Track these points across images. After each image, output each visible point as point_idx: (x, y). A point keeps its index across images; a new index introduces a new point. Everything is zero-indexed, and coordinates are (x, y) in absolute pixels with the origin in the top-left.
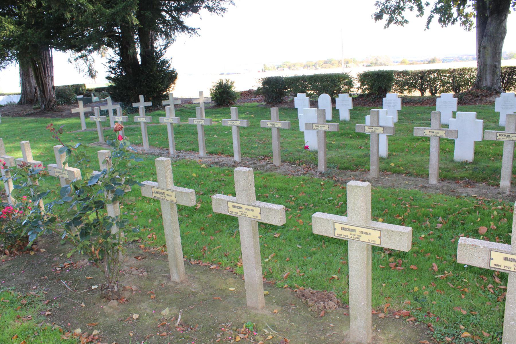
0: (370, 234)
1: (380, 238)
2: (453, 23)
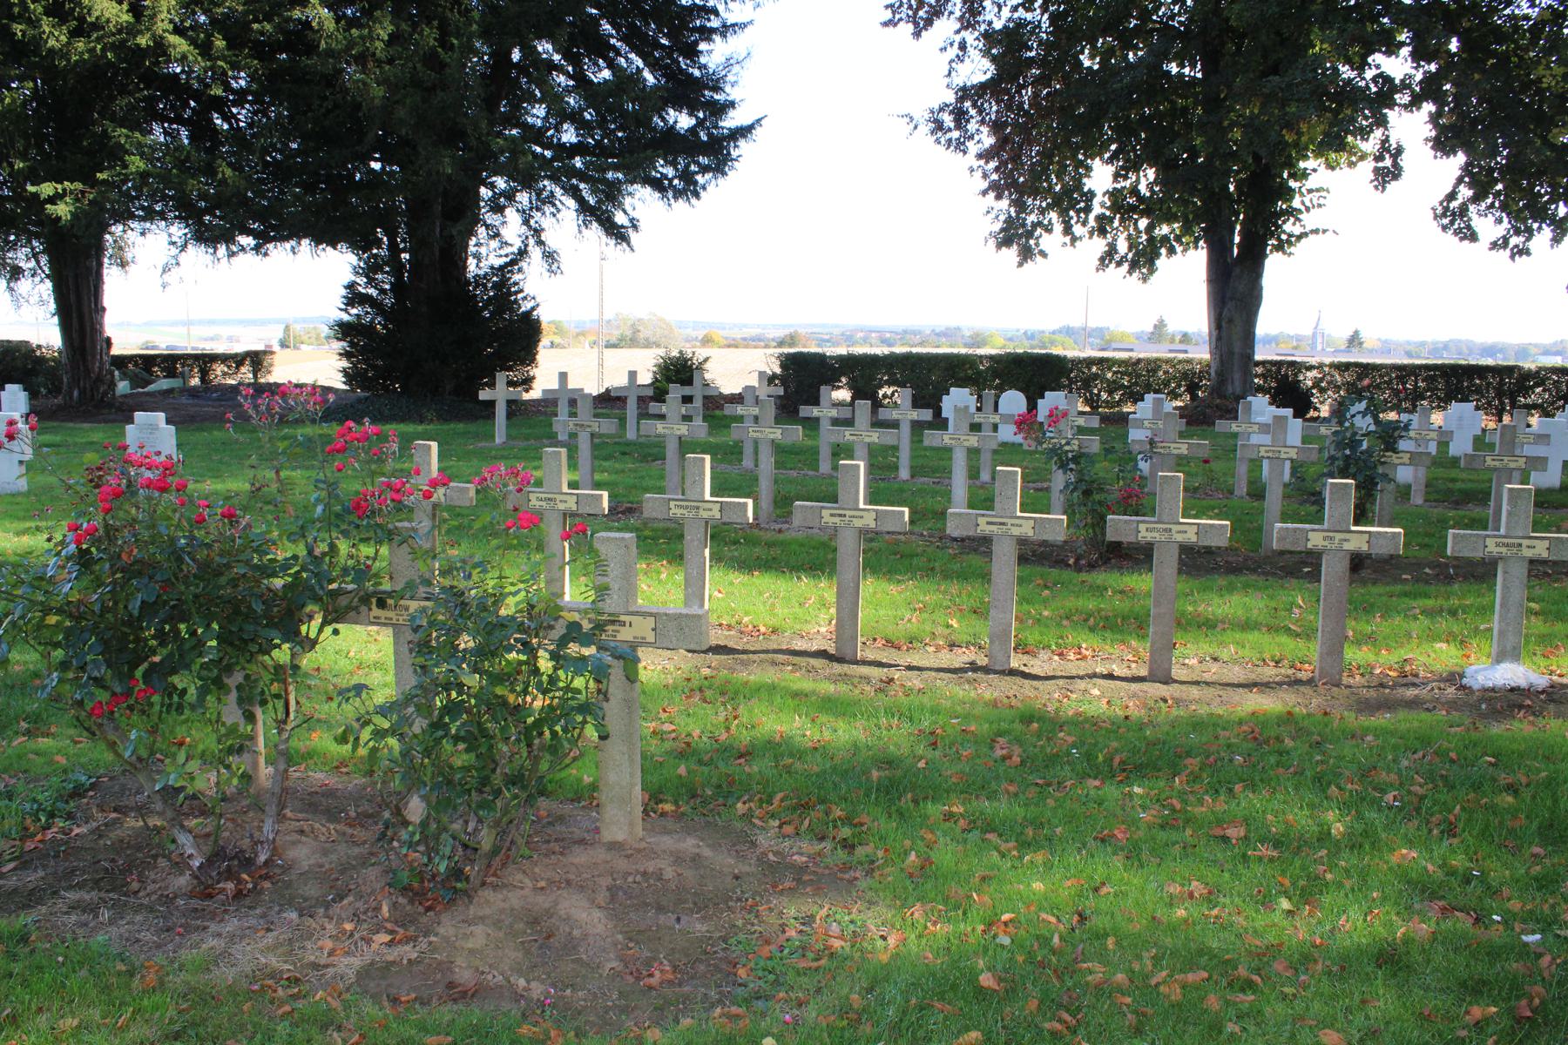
2: (1119, 264)
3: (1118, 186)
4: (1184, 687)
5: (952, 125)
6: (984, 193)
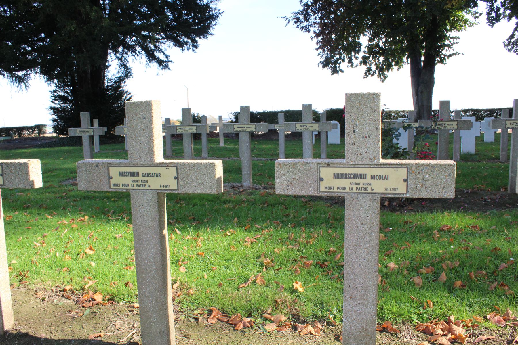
1: (176, 178)
2: (372, 75)
3: (371, 43)
5: (303, 20)
6: (317, 49)
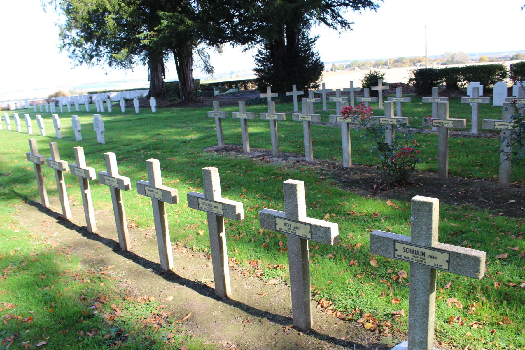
0: (436, 258)
1: (448, 262)
4: (316, 341)
